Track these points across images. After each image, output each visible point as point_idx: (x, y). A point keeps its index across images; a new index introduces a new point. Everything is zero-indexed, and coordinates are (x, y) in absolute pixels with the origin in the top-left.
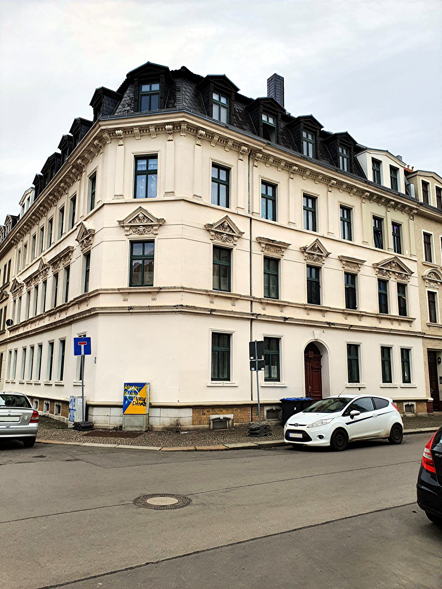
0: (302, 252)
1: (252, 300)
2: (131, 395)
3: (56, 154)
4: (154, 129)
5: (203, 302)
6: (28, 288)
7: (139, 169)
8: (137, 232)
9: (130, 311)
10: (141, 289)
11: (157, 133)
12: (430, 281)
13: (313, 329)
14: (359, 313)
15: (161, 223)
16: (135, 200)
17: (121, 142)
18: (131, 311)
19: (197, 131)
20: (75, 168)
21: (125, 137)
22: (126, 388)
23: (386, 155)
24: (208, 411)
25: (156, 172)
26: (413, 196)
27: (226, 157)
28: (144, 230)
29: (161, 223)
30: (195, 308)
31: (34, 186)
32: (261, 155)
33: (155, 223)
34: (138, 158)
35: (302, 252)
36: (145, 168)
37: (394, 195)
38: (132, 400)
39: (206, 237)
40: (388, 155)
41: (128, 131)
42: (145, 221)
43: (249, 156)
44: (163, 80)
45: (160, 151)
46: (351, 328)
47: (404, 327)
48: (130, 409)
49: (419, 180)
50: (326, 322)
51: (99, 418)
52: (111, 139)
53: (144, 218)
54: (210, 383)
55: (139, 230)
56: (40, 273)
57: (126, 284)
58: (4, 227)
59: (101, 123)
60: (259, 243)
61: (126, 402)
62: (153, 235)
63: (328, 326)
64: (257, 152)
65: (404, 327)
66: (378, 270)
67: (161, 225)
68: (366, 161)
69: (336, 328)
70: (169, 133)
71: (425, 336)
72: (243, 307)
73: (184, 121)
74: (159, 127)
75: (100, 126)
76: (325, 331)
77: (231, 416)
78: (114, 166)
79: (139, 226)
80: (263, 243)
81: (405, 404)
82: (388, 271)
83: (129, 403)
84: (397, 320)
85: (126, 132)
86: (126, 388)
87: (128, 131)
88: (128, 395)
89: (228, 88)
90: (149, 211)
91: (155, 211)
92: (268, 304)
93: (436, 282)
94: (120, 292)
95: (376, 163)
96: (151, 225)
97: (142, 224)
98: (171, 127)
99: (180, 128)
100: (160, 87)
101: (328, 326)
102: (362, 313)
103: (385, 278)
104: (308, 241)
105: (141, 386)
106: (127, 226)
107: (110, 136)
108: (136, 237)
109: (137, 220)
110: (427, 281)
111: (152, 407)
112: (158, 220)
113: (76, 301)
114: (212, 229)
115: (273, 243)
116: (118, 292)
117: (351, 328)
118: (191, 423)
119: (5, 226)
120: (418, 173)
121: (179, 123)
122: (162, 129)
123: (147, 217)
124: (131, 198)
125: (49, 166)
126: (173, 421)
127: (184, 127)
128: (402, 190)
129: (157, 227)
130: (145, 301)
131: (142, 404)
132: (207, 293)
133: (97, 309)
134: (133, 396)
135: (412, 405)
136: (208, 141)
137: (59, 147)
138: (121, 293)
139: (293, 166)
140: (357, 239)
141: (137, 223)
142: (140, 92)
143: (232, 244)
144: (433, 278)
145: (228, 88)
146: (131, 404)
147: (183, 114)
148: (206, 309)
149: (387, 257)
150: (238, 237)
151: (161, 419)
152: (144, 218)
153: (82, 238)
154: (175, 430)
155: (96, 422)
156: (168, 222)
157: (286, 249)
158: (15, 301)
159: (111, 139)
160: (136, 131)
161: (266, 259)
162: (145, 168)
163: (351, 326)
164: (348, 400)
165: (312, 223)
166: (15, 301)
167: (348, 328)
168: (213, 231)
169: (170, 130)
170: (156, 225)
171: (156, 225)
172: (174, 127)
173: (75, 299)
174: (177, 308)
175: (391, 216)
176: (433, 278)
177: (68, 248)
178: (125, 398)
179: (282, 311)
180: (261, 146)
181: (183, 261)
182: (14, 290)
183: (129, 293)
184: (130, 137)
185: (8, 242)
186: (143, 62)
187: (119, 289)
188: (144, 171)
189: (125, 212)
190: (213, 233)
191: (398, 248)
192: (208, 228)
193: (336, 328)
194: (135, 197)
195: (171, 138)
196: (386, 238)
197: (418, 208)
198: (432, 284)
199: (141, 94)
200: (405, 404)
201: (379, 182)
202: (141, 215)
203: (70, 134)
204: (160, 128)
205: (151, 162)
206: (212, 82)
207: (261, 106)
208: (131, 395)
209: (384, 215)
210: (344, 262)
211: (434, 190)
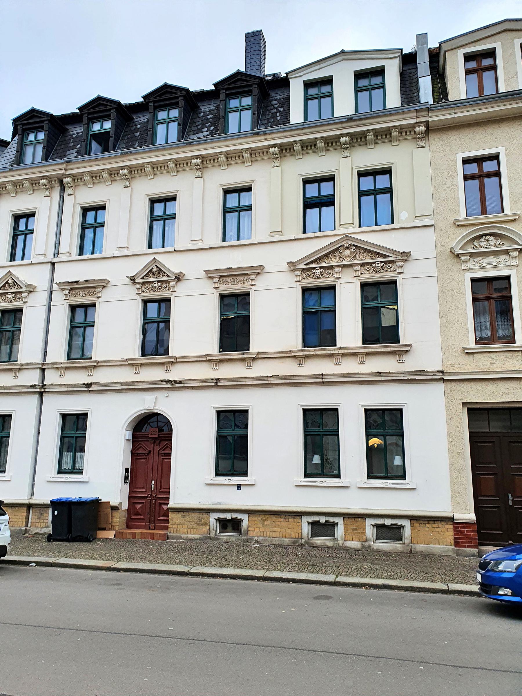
4: (300, 147)
7: (156, 214)
10: (7, 365)
11: (112, 179)
15: (405, 256)
16: (225, 244)
17: (346, 153)
21: (203, 168)
25: (250, 208)
28: (159, 286)
33: (24, 289)
34: (153, 202)
44: (256, 91)
45: (108, 201)
53: (159, 273)
57: (299, 345)
63: (169, 386)
69: (193, 388)
70: (419, 138)
85: (328, 143)
91: (172, 264)
94: (291, 356)
98: (347, 139)
99: (391, 136)
108: (311, 282)
112: (27, 286)
116: (204, 359)
121: (411, 126)
122: (410, 132)
124: (145, 249)
129: (101, 289)
142: (227, 108)
152: (159, 273)
156: (267, 269)
160: (321, 144)
167: (213, 384)
169: (422, 134)
172: (203, 161)
183: (142, 365)
184: (406, 139)
186: (233, 71)
187: (206, 356)
193: (193, 388)
194: (224, 240)
196: (322, 284)
204: (113, 173)
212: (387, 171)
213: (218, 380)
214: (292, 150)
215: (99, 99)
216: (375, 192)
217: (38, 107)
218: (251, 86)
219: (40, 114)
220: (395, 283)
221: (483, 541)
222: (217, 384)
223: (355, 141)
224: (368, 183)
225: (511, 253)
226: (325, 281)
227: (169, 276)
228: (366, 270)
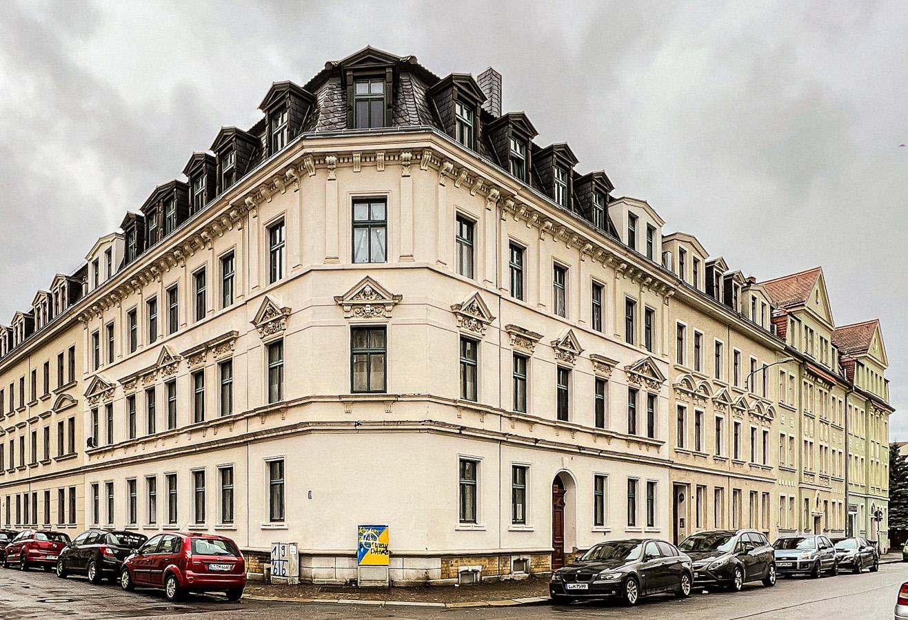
0: (553, 348)
1: (501, 413)
2: (368, 541)
3: (177, 184)
5: (448, 416)
6: (128, 392)
8: (361, 314)
9: (357, 427)
12: (682, 391)
13: (562, 455)
14: (610, 434)
15: (397, 299)
17: (332, 175)
18: (358, 427)
19: (442, 164)
20: (235, 209)
22: (361, 531)
23: (644, 208)
24: (456, 562)
26: (670, 269)
27: (473, 206)
28: (372, 311)
29: (397, 301)
30: (444, 424)
31: (121, 231)
32: (512, 204)
33: (388, 300)
35: (553, 348)
36: (369, 215)
37: (653, 269)
38: (370, 547)
39: (452, 323)
40: (646, 208)
41: (345, 157)
42: (374, 298)
43: (497, 203)
46: (601, 454)
47: (652, 453)
48: (368, 558)
49: (677, 245)
50: (577, 446)
51: (319, 571)
52: (316, 169)
53: (371, 294)
54: (459, 526)
55: (364, 311)
56: (158, 370)
58: (49, 295)
59: (305, 143)
60: (509, 333)
61: (362, 550)
62: (385, 319)
63: (578, 451)
64: (509, 199)
65: (652, 453)
66: (629, 375)
67: (396, 304)
68: (619, 215)
70: (404, 165)
71: (673, 466)
72: (492, 424)
73: (430, 148)
74: (389, 154)
75: (303, 147)
76: (575, 457)
77: (479, 568)
78: (315, 213)
79: (364, 305)
80: (514, 334)
81: (514, 558)
82: (640, 376)
83: (366, 551)
84: (646, 443)
86: (361, 531)
87: (345, 157)
88: (363, 541)
89: (474, 96)
90: (380, 283)
91: (389, 283)
92: (518, 420)
93: (687, 393)
95: (633, 218)
96: (382, 304)
97: (371, 303)
98: (409, 155)
99: (421, 159)
100: (386, 88)
101: (578, 451)
102: (612, 435)
103: (636, 386)
104: (561, 332)
105: (381, 528)
106: (347, 305)
107: (315, 164)
108: (360, 320)
109: (361, 295)
110: (679, 391)
111: (392, 556)
112: (394, 297)
113: (257, 412)
114: (460, 312)
115: (524, 333)
116: (338, 400)
117: (601, 454)
118: (440, 577)
119: (50, 292)
120: (677, 237)
123: (376, 292)
125: (159, 202)
126: (421, 574)
127: (427, 156)
128: (658, 259)
130: (375, 413)
131: (383, 552)
132: (341, 400)
133: (310, 424)
134: (371, 542)
135: (525, 561)
136: (452, 179)
137: (185, 172)
138: (342, 402)
139: (546, 221)
140: (608, 331)
141: (363, 300)
143: (480, 334)
144: (685, 388)
145: (474, 96)
146: (369, 552)
147: (429, 137)
148: (454, 426)
149: (640, 357)
150: (488, 324)
151: (405, 572)
153: (262, 320)
154: (424, 587)
155: (317, 576)
157: (536, 341)
158: (95, 411)
159: (316, 169)
161: (516, 356)
162: (369, 215)
163: (602, 451)
164: (628, 546)
165: (561, 306)
166: (95, 411)
167: (458, 431)
168: (461, 314)
169: (408, 161)
170: (389, 304)
171: (389, 304)
173: (255, 410)
174: (423, 425)
175: (648, 298)
176: (685, 388)
177: (231, 333)
178: (361, 546)
179: (231, 430)
180: (514, 189)
181: (421, 359)
182: (91, 394)
185: (69, 319)
186: (363, 47)
188: (365, 222)
189: (346, 284)
190: (460, 318)
191: (649, 346)
192: (339, 301)
195: (407, 174)
197: (676, 287)
198: (682, 395)
199: (357, 97)
200: (514, 558)
201: (633, 246)
202: (368, 289)
203: (212, 154)
205: (375, 207)
206: (456, 86)
207: (510, 125)
208: (368, 541)
209: (637, 297)
210: (596, 364)
211: (349, 233)
212: (383, 200)
213: (463, 428)
214: (350, 160)
215: (369, 51)
216: (370, 225)
217: (376, 46)
218: (384, 68)
219: (381, 57)
220: (384, 328)
221: (214, 591)
222: (461, 432)
223: (341, 161)
224: (362, 213)
225: (387, 307)
226: (375, 320)
227: (383, 298)
228: (356, 313)
